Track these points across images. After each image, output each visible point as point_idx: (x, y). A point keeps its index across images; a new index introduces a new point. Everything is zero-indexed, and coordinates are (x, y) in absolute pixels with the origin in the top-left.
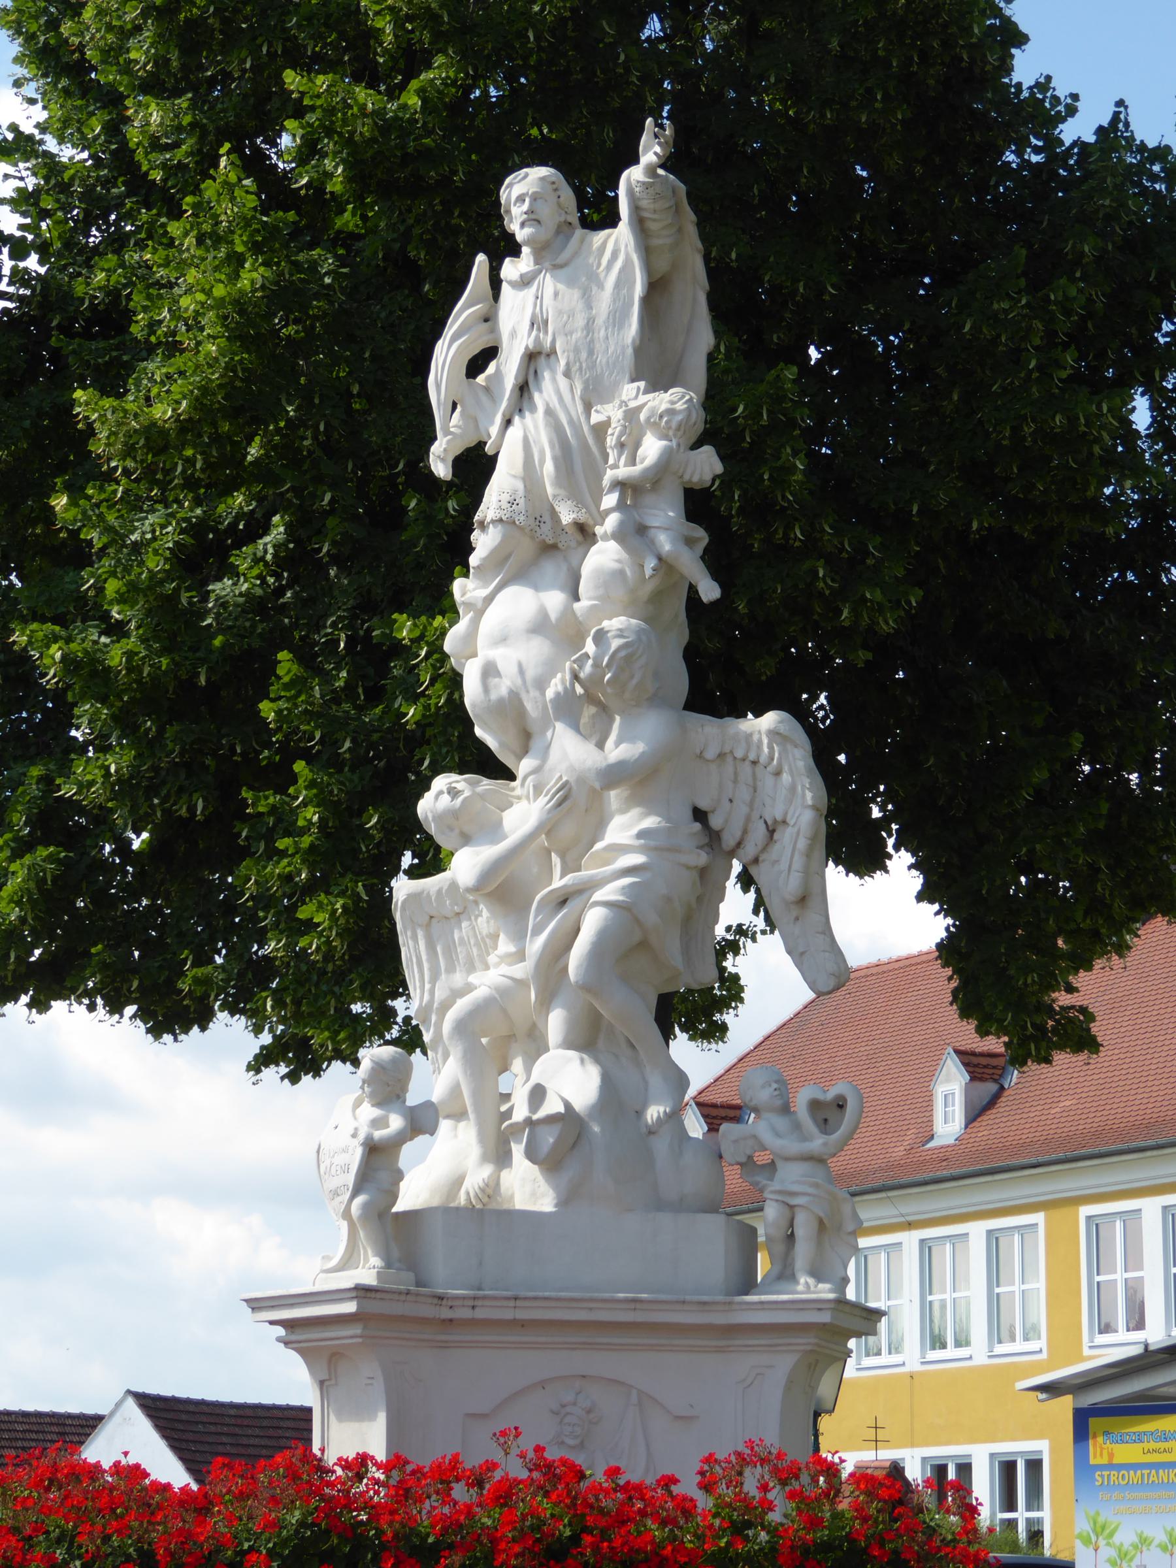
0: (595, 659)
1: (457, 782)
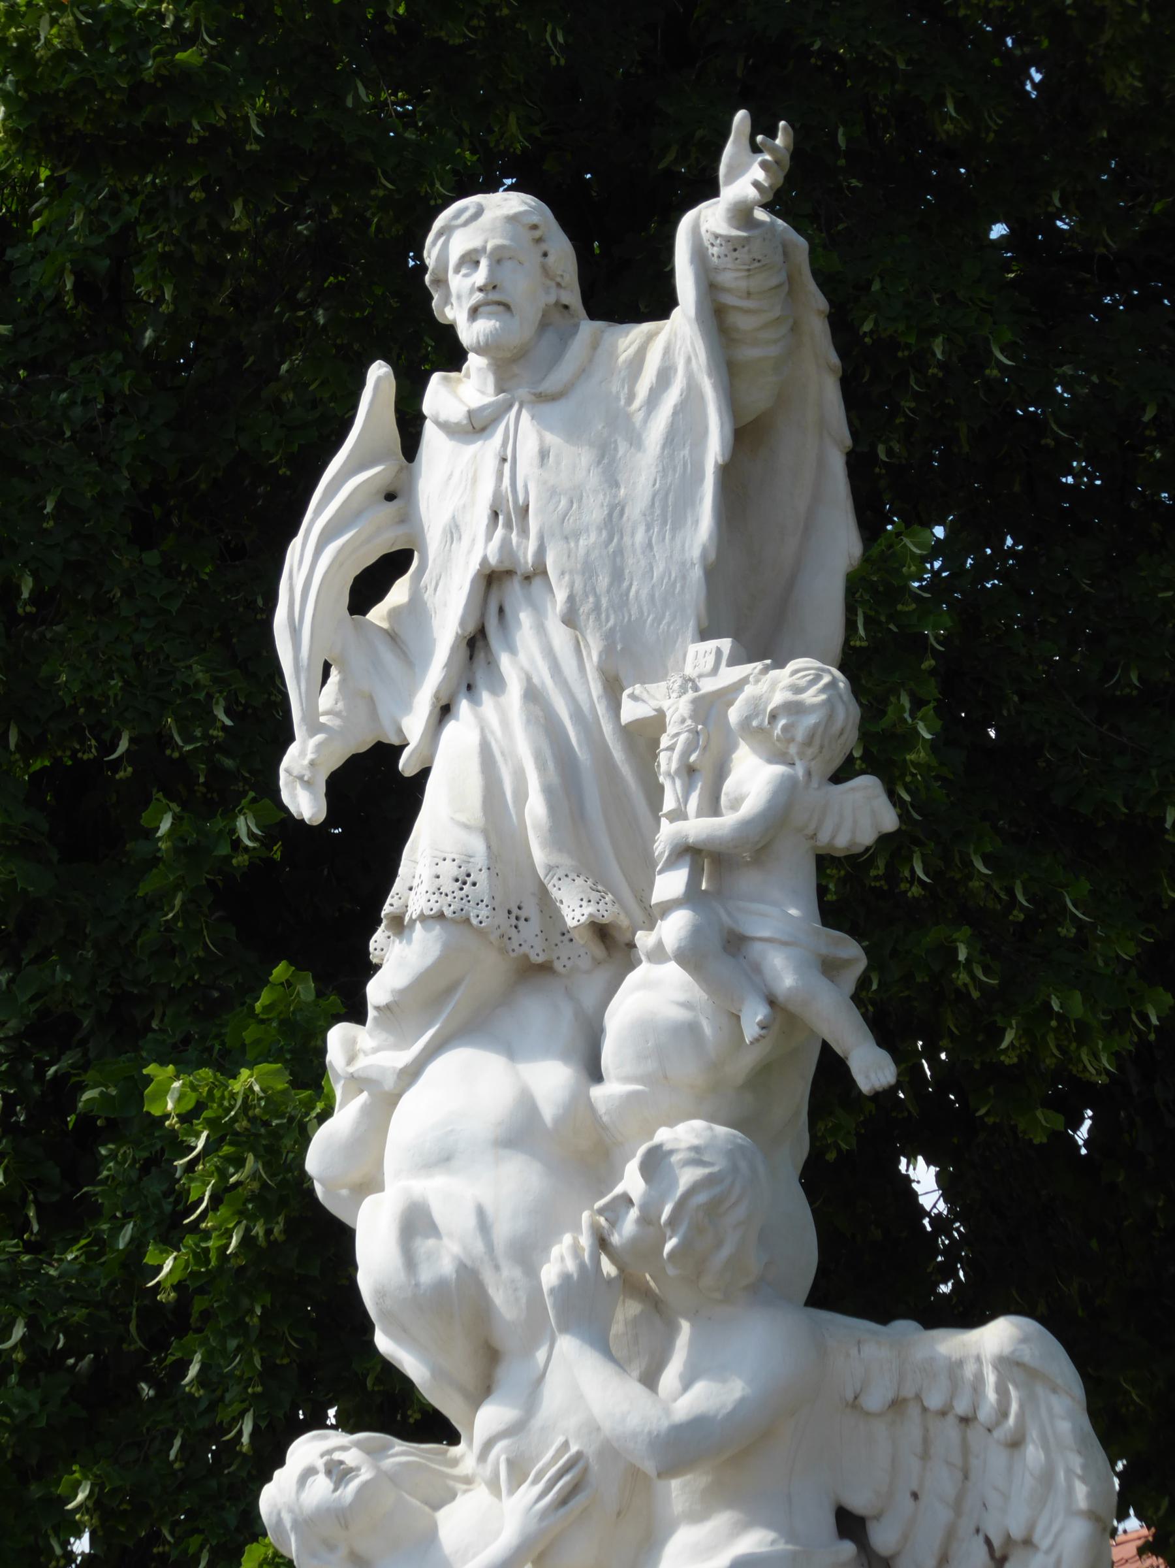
0: (644, 1208)
1: (343, 1448)
